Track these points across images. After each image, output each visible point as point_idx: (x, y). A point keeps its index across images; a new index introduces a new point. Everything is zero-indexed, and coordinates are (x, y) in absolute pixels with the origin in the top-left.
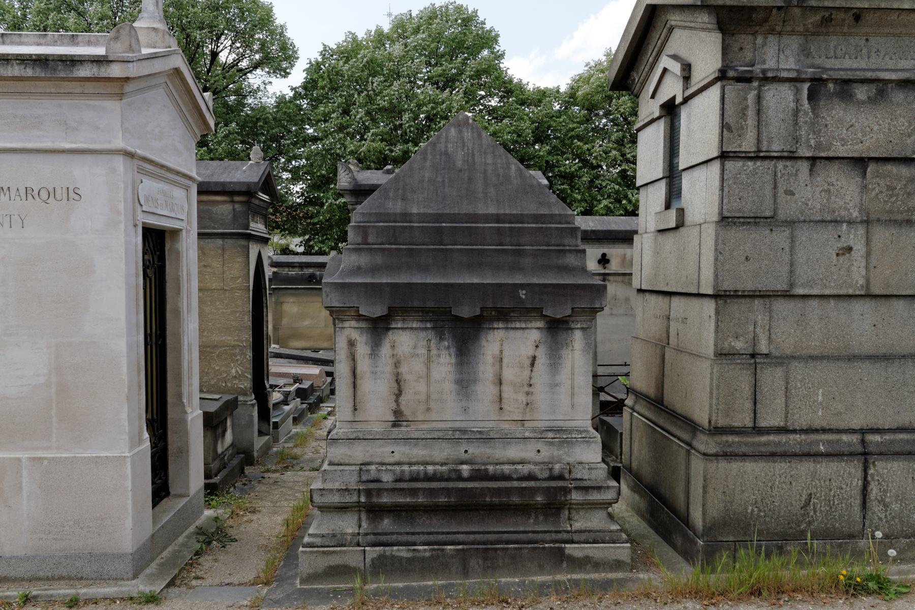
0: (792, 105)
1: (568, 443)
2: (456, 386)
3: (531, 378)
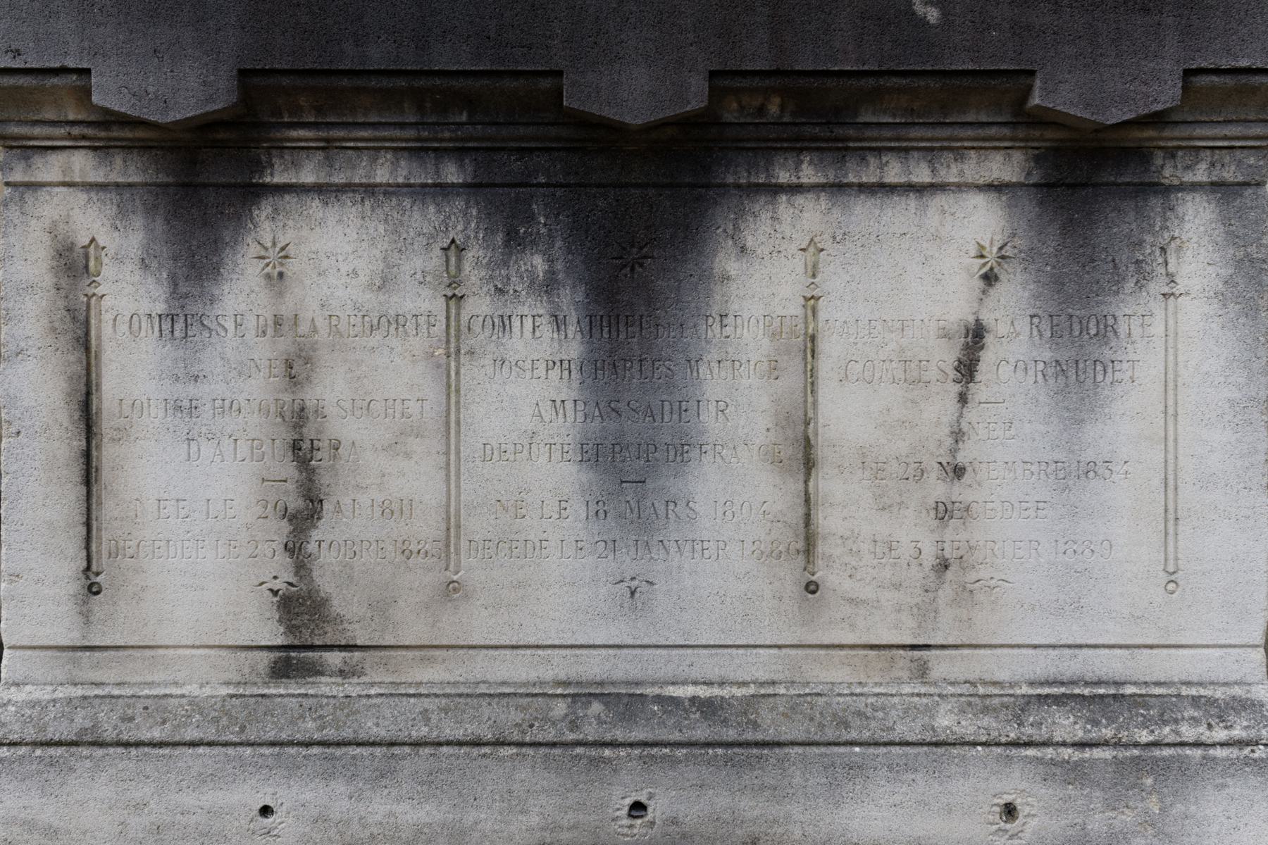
1: (1161, 769)
2: (586, 476)
3: (958, 435)
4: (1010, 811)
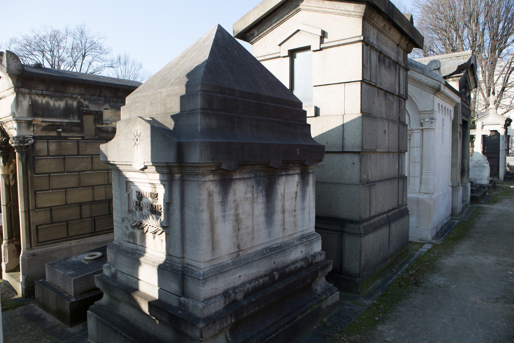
4: (240, 276)
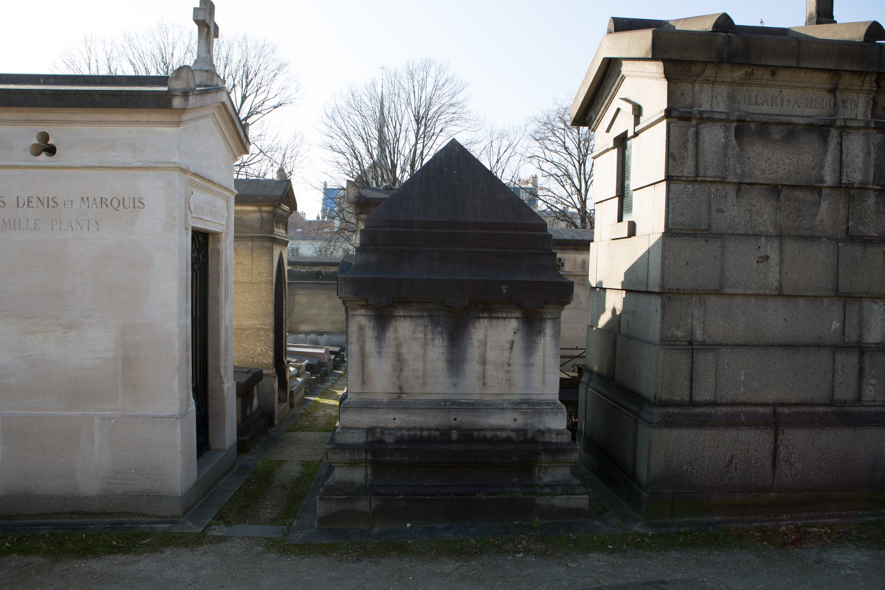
0: (723, 140)
